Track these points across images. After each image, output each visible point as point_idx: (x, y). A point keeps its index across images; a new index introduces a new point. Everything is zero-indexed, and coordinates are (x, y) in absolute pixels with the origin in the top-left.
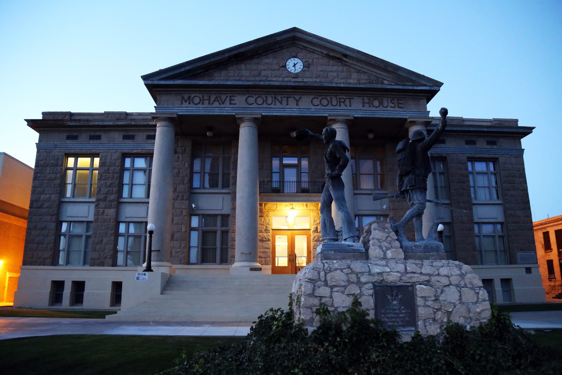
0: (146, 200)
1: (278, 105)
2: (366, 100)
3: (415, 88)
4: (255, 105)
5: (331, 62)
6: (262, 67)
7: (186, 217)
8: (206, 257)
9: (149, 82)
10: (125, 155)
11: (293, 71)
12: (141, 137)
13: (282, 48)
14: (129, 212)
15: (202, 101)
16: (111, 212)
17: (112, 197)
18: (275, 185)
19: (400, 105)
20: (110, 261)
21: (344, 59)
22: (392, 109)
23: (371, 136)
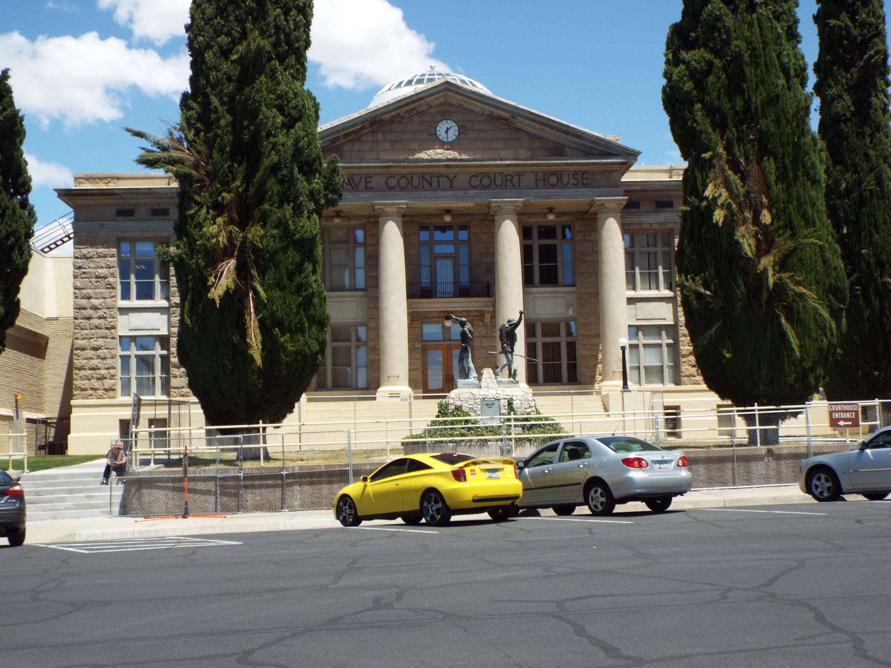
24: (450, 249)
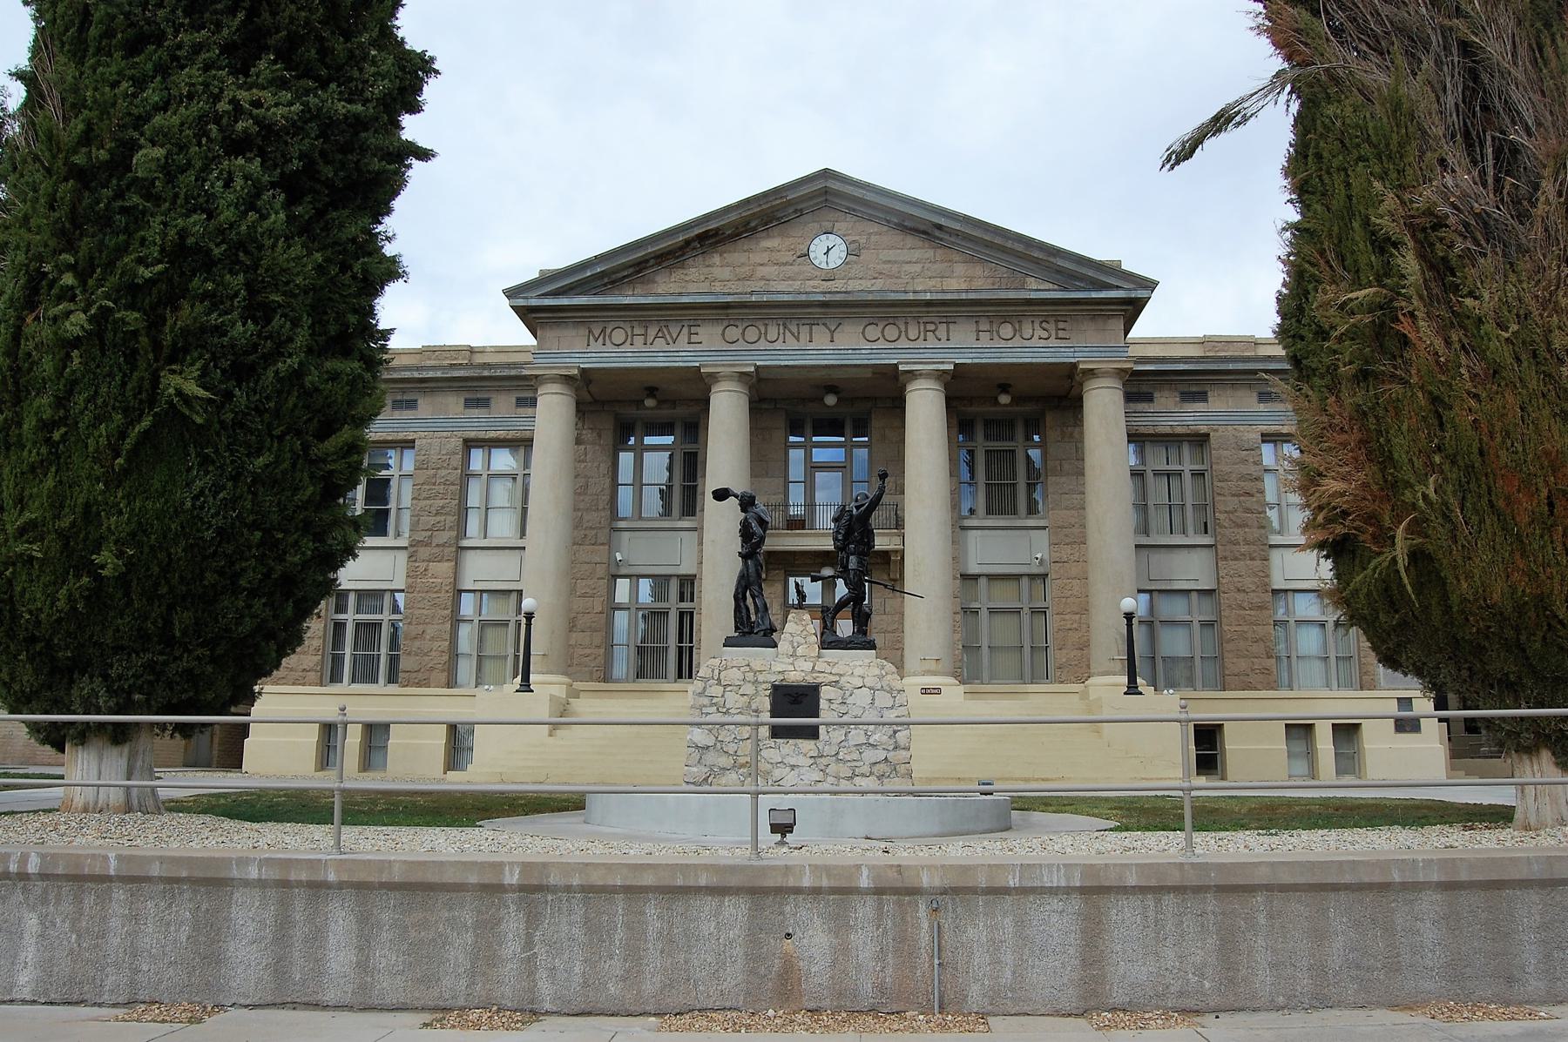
0: (520, 543)
1: (792, 343)
2: (984, 326)
3: (1094, 295)
4: (741, 345)
5: (910, 240)
6: (756, 258)
7: (602, 582)
8: (647, 664)
9: (521, 302)
10: (469, 444)
11: (824, 266)
12: (503, 405)
13: (800, 213)
14: (479, 570)
15: (630, 339)
16: (445, 568)
17: (444, 537)
18: (796, 511)
19: (1061, 334)
20: (443, 677)
21: (937, 233)
22: (1043, 343)
23: (1004, 399)
24: (837, 455)
